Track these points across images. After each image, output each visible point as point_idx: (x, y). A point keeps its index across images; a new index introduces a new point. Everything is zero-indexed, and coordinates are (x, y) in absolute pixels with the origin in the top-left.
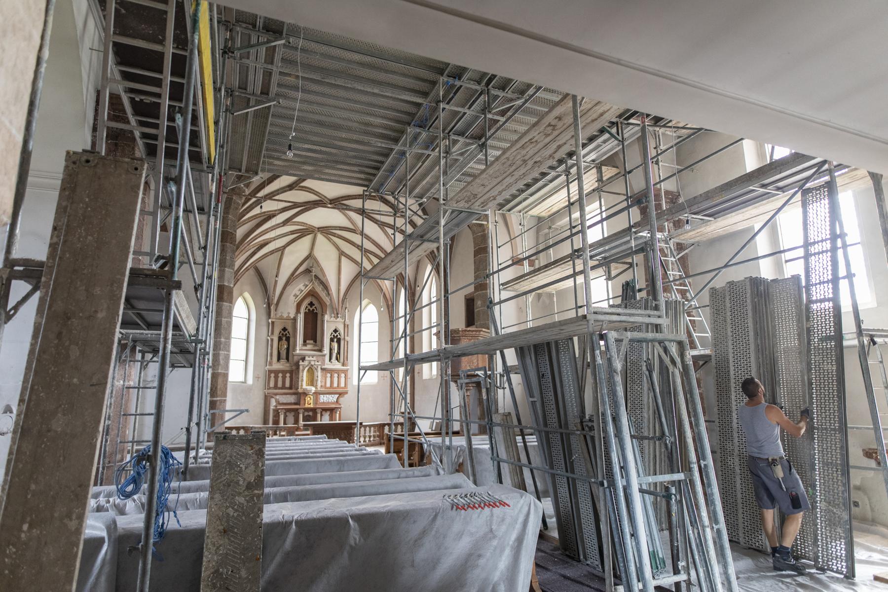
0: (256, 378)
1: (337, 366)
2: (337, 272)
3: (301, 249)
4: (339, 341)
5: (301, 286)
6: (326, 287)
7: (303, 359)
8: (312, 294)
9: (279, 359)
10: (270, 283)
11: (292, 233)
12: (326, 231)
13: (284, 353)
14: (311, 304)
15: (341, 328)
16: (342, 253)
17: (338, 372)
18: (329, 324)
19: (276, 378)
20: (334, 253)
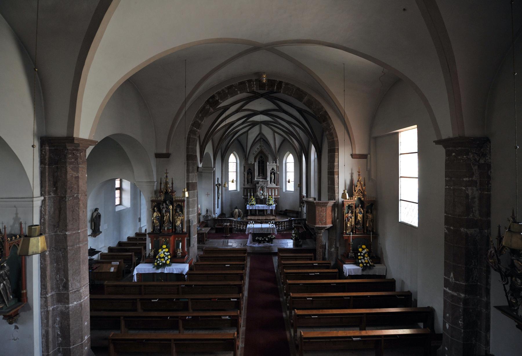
1: (274, 185)
2: (274, 139)
3: (253, 133)
5: (258, 147)
7: (258, 183)
9: (248, 183)
10: (245, 148)
11: (249, 125)
12: (266, 123)
13: (250, 181)
14: (261, 157)
15: (275, 168)
16: (275, 132)
17: (275, 188)
18: (270, 166)
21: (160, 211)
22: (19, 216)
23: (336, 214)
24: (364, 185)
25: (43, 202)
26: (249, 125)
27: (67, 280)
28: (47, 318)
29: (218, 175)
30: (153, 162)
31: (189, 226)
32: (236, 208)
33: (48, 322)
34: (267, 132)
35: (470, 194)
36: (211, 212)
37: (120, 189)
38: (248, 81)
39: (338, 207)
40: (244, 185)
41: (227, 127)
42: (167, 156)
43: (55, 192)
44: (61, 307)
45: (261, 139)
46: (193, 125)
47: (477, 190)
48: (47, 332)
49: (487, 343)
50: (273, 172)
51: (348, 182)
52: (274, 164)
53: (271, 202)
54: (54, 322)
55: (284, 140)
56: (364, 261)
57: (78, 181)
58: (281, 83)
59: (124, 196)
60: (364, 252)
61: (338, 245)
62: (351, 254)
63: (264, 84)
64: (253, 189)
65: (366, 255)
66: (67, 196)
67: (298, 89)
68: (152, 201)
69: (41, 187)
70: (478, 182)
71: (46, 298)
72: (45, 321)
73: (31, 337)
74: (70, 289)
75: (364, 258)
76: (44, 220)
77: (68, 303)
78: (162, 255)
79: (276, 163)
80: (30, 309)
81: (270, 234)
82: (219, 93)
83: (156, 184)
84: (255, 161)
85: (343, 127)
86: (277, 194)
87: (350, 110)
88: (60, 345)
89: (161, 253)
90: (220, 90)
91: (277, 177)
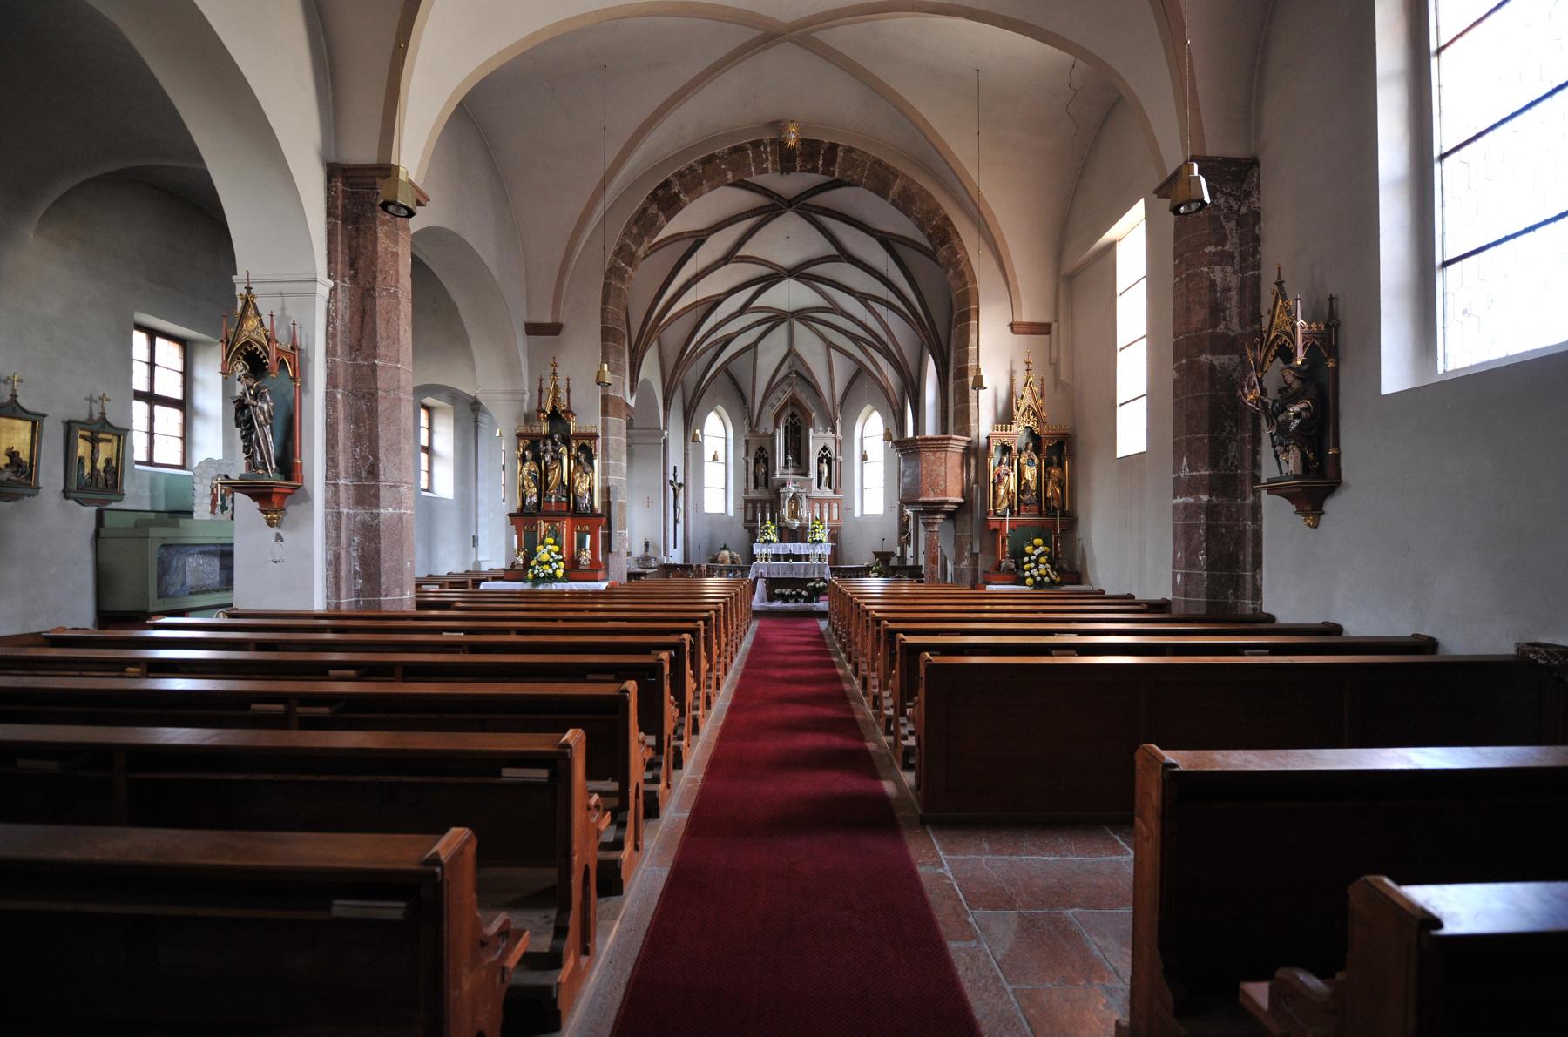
0: (736, 508)
2: (830, 373)
4: (829, 462)
6: (814, 388)
7: (784, 485)
8: (794, 402)
10: (747, 390)
11: (760, 323)
12: (803, 315)
13: (762, 479)
14: (793, 416)
16: (830, 345)
17: (829, 501)
18: (817, 440)
19: (755, 509)
20: (819, 346)
21: (537, 459)
22: (288, 313)
23: (972, 474)
24: (1042, 396)
25: (333, 290)
26: (760, 323)
27: (377, 458)
28: (338, 528)
29: (675, 458)
30: (521, 340)
31: (609, 503)
32: (725, 548)
33: (338, 537)
34: (809, 346)
35: (1219, 281)
36: (657, 548)
37: (428, 450)
38: (751, 143)
39: (975, 454)
40: (746, 491)
41: (701, 310)
42: (554, 329)
43: (354, 278)
44: (362, 514)
45: (796, 371)
46: (617, 254)
47: (1235, 272)
48: (337, 557)
49: (1257, 594)
50: (826, 458)
51: (1003, 394)
52: (829, 434)
53: (822, 535)
54: (350, 541)
55: (859, 372)
56: (1035, 572)
57: (396, 262)
58: (833, 147)
59: (437, 469)
60: (1037, 552)
61: (976, 550)
62: (1007, 563)
63: (793, 150)
64: (771, 502)
65: (1043, 560)
66: (379, 286)
67: (878, 162)
68: (520, 436)
69: (329, 262)
70: (1237, 254)
71: (336, 486)
72: (334, 534)
73: (309, 556)
74: (382, 478)
75: (1037, 567)
76: (335, 328)
77: (377, 507)
78: (545, 557)
79: (834, 430)
80: (307, 498)
81: (812, 580)
82: (680, 175)
83: (527, 397)
84: (776, 426)
85: (984, 248)
86: (835, 517)
87: (1004, 201)
88: (359, 593)
89: (543, 553)
90: (682, 167)
91: (833, 469)
